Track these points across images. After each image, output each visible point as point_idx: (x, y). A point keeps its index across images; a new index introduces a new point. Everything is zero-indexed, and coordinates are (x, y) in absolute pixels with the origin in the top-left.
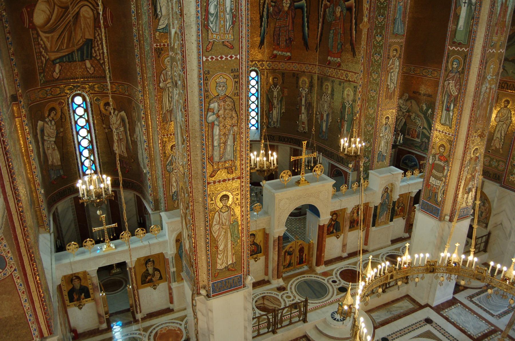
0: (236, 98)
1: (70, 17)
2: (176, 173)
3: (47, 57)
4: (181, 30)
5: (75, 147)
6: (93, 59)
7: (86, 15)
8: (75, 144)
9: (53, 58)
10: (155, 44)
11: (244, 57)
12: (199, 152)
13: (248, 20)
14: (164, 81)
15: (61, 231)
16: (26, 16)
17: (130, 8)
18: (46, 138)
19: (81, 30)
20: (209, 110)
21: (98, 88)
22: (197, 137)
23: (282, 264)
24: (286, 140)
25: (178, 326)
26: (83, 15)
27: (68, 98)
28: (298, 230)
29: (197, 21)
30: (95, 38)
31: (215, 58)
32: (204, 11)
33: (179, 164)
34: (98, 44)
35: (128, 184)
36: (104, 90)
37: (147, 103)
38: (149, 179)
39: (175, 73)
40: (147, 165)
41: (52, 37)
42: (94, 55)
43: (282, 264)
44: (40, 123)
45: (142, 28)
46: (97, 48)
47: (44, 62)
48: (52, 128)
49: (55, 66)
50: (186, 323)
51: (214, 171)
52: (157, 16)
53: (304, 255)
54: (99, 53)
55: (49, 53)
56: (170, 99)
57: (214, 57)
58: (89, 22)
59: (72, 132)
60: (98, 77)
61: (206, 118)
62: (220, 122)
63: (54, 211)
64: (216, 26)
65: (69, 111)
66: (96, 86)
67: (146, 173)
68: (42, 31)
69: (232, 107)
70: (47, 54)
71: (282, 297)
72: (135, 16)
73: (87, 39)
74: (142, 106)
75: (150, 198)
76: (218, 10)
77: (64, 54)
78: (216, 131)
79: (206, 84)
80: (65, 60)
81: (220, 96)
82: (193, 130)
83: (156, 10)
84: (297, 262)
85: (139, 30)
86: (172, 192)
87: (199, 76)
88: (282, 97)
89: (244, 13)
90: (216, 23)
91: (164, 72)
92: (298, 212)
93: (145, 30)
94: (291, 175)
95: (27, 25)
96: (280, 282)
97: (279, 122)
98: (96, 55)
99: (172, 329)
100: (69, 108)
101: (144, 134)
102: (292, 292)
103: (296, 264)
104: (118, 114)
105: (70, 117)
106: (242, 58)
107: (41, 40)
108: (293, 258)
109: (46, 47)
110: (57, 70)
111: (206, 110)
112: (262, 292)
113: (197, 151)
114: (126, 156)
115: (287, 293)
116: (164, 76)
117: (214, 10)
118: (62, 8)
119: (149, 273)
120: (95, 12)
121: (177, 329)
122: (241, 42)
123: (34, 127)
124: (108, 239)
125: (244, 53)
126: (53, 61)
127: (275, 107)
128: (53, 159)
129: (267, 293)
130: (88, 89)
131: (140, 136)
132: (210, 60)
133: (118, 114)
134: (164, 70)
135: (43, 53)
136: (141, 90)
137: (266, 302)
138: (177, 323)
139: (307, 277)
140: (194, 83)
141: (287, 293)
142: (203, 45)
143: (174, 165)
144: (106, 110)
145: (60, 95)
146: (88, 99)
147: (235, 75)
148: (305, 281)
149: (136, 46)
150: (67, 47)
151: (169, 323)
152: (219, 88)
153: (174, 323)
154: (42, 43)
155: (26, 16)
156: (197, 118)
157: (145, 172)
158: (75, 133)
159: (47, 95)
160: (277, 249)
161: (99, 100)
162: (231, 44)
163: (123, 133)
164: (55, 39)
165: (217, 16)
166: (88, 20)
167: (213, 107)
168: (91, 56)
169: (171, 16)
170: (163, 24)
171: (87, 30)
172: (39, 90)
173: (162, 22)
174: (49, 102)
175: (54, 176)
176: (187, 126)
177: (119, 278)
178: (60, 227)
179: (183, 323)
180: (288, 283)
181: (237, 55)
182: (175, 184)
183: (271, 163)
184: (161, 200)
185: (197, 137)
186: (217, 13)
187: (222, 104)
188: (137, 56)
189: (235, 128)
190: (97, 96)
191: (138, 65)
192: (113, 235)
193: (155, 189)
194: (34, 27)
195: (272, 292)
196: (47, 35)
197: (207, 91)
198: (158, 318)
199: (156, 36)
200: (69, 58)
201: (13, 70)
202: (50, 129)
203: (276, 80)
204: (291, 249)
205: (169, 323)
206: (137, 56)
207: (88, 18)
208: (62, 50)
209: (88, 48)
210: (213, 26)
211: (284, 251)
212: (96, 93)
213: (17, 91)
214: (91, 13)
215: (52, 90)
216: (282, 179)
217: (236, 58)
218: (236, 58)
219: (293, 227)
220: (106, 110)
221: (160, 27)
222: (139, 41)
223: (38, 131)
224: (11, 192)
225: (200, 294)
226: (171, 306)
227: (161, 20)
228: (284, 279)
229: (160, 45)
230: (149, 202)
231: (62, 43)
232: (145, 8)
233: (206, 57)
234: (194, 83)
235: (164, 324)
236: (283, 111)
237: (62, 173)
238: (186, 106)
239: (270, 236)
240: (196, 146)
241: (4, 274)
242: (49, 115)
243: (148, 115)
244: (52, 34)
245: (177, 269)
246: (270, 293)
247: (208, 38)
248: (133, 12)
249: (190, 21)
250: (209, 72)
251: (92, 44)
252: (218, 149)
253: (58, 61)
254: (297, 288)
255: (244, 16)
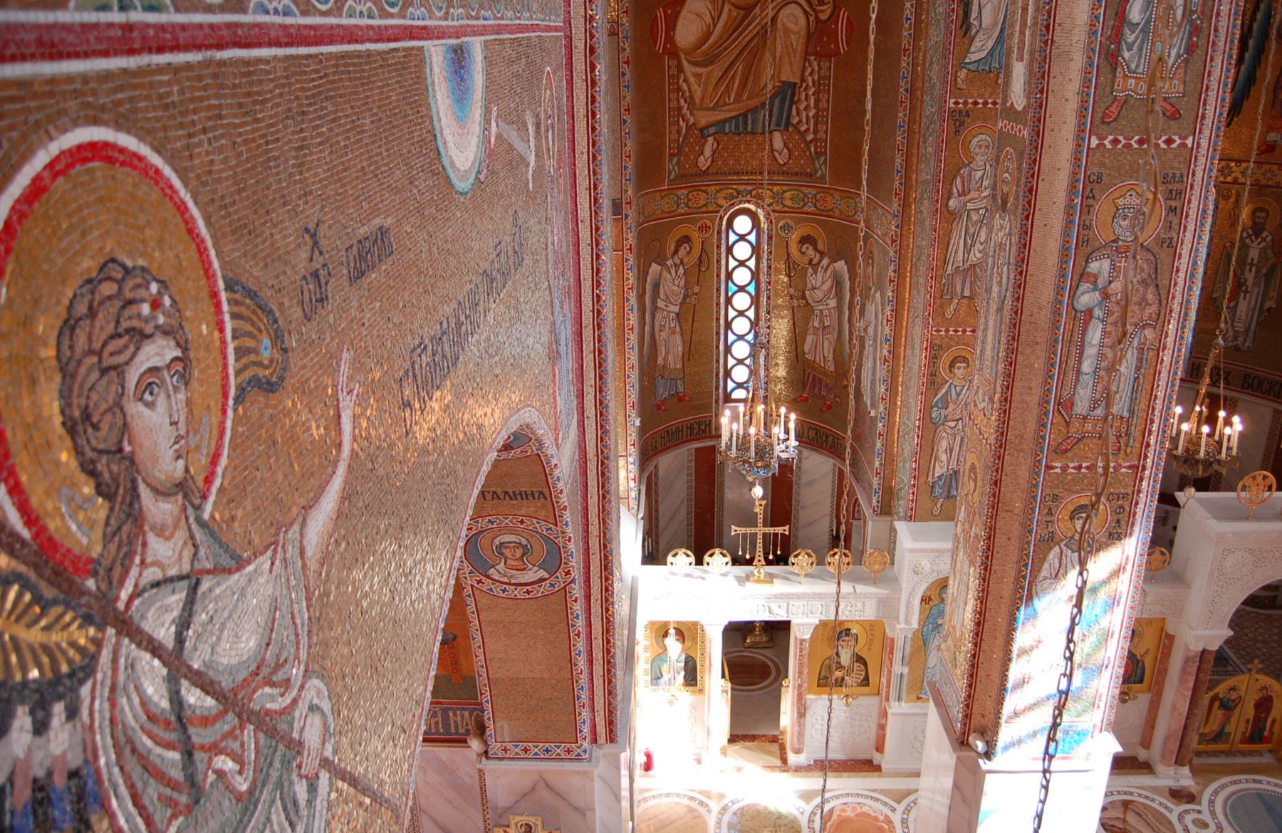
0: (1164, 256)
1: (754, 28)
2: (952, 428)
3: (692, 121)
4: (1043, 64)
5: (718, 334)
6: (790, 129)
7: (791, 26)
8: (718, 326)
9: (703, 122)
10: (952, 101)
11: (1204, 143)
12: (1036, 384)
13: (1232, 41)
14: (960, 195)
15: (657, 519)
16: (662, 25)
17: (902, 8)
18: (660, 304)
19: (775, 58)
20: (1083, 276)
21: (791, 199)
22: (1037, 343)
23: (1199, 729)
24: (1266, 386)
25: (887, 811)
26: (783, 24)
27: (721, 218)
28: (1259, 645)
29: (1090, 43)
30: (803, 80)
31: (1123, 141)
32: (1113, 17)
33: (975, 405)
34: (807, 95)
35: (824, 438)
36: (804, 205)
37: (908, 246)
38: (880, 435)
39: (1006, 175)
40: (883, 399)
41: (709, 75)
42: (795, 121)
43: (1199, 729)
44: (655, 268)
45: (925, 58)
46: (805, 103)
47: (684, 131)
48: (676, 282)
49: (706, 141)
50: (908, 810)
51: (1069, 438)
52: (968, 29)
53: (1269, 720)
54: (807, 117)
55: (695, 112)
56: (969, 242)
57: (1121, 138)
58: (794, 43)
59: (718, 297)
60: (797, 174)
61: (1072, 297)
62: (1108, 313)
63: (651, 473)
64: (1140, 56)
65: (719, 247)
66: (787, 195)
67: (876, 417)
68: (689, 62)
69: (1150, 275)
70: (691, 114)
71: (1181, 818)
72: (910, 29)
73: (783, 82)
74: (895, 252)
75: (875, 482)
76: (1151, 14)
77: (728, 115)
78: (1095, 334)
79: (1087, 209)
80: (727, 131)
81: (1120, 243)
82: (1030, 323)
83: (967, 14)
84: (1244, 734)
85: (915, 64)
86: (933, 475)
87: (1072, 187)
88: (1273, 267)
89: (1223, 24)
90: (1140, 49)
91: (965, 171)
92: (1267, 597)
93: (931, 63)
94: (1274, 487)
95: (660, 47)
96: (1185, 779)
97: (1251, 335)
98: (800, 121)
99: (869, 815)
100: (719, 240)
101: (888, 321)
102: (1213, 814)
103: (1238, 737)
104: (828, 266)
105: (719, 261)
106: (1198, 147)
107: (685, 80)
108: (1234, 719)
109: (691, 97)
110: (708, 151)
111: (1076, 277)
112: (1125, 789)
113: (1032, 380)
114: (832, 369)
115: (1199, 812)
116: (963, 182)
117: (1140, 14)
118: (740, 8)
119: (839, 663)
120: (811, 19)
121: (881, 818)
122: (1205, 100)
123: (642, 275)
124: (762, 559)
125: (1207, 133)
126: (702, 130)
127: (1246, 292)
128: (667, 353)
129: (1140, 795)
130: (768, 201)
131: (876, 325)
132: (1109, 146)
133: (828, 266)
134: (965, 165)
135: (685, 110)
136: (899, 211)
137: (1131, 818)
138: (885, 804)
139: (1269, 783)
140: (1054, 203)
141: (1199, 812)
142: (1097, 106)
143: (950, 409)
144: (803, 253)
145: (705, 209)
146: (764, 224)
147: (1171, 191)
148: (1259, 795)
149: (902, 102)
150: (738, 99)
151: (866, 797)
152: (1121, 223)
153: (877, 800)
154: (685, 87)
155: (662, 25)
156: (1047, 294)
157: (873, 414)
158: (722, 299)
159: (678, 206)
160: (1191, 684)
161: (786, 227)
162: (1173, 106)
163: (835, 314)
164: (714, 80)
165: (1145, 31)
166: (793, 37)
167: (1095, 271)
168: (788, 124)
169: (1017, 29)
170: (980, 50)
171: (786, 59)
172: (664, 193)
173: (979, 44)
174: (681, 222)
175: (662, 392)
176: (1016, 313)
177: (762, 658)
178: (656, 510)
179: (900, 808)
180: (1206, 786)
181: (1186, 138)
182: (944, 457)
183: (1220, 443)
184: (900, 490)
185: (1037, 343)
186: (1148, 22)
187: (1122, 265)
188: (900, 127)
189: (1148, 333)
190: (788, 218)
191: (899, 150)
192: (775, 553)
193: (889, 460)
194: (673, 51)
195: (1155, 797)
196: (699, 70)
197: (1085, 226)
198: (840, 777)
199: (959, 80)
200: (737, 126)
201: (623, 145)
202: (673, 284)
203: (1264, 215)
204: (1234, 696)
205: (866, 797)
206: (900, 127)
207: (795, 33)
208: (725, 104)
209: (784, 100)
210: (1132, 56)
211: (1211, 694)
212: (786, 212)
213: (623, 191)
214: (802, 20)
215: (690, 196)
216: (1243, 494)
217: (1183, 145)
218: (1183, 145)
219: (1246, 635)
220: (803, 253)
221: (974, 57)
222: (912, 91)
223: (648, 287)
224: (593, 408)
225: (968, 744)
226: (877, 757)
227: (977, 39)
228: (1195, 771)
229: (965, 103)
230: (868, 492)
231: (728, 90)
232: (941, 9)
233: (1099, 139)
234: (1054, 203)
235: (852, 795)
236: (1268, 305)
237: (681, 389)
238: (1023, 262)
239: (1177, 642)
240: (1032, 365)
241: (552, 585)
242: (676, 252)
243: (906, 277)
244: (710, 68)
245: (911, 668)
246: (1147, 798)
247: (1112, 88)
248: (908, 19)
249: (1068, 43)
250: (1100, 178)
251: (793, 95)
252: (1091, 383)
253: (712, 130)
254: (1233, 807)
255: (1222, 31)
